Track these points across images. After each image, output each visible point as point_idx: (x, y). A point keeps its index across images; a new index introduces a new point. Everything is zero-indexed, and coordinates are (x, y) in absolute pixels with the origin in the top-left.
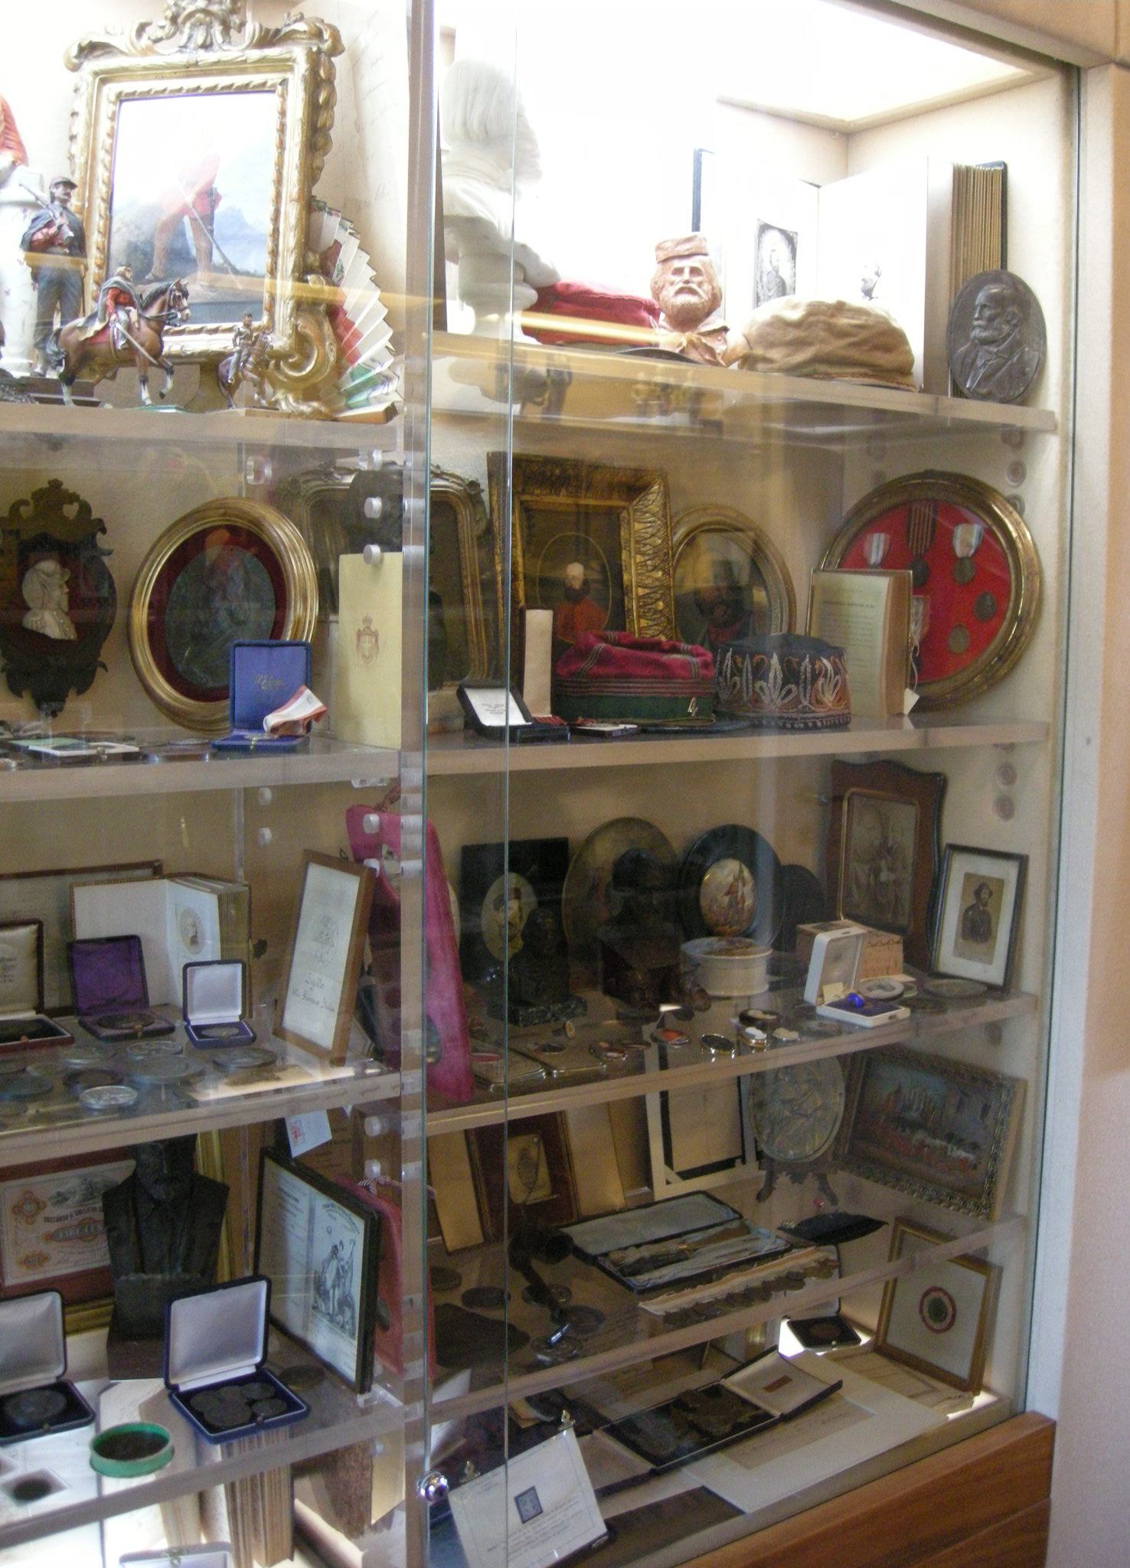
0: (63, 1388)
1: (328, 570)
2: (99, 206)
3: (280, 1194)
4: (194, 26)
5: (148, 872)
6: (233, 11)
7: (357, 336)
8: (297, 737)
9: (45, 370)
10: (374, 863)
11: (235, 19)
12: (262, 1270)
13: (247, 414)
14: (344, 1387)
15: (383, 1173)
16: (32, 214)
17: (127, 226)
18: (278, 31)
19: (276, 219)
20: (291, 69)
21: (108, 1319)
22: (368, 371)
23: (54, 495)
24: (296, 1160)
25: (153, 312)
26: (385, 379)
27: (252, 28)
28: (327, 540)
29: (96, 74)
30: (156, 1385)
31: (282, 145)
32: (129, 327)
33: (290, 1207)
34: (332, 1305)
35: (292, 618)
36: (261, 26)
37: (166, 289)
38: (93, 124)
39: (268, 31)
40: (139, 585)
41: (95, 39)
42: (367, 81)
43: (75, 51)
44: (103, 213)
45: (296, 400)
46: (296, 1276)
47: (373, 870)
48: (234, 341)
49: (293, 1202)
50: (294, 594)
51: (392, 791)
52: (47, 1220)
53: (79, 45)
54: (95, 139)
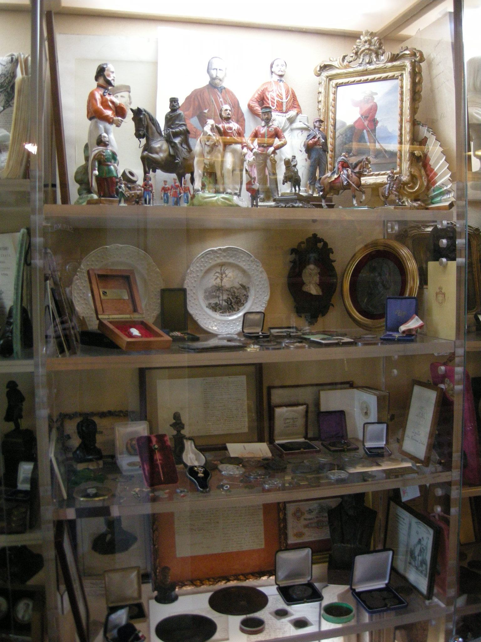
0: (310, 585)
1: (422, 267)
2: (331, 128)
3: (397, 516)
4: (364, 55)
5: (348, 385)
6: (380, 48)
7: (436, 174)
8: (413, 335)
9: (313, 193)
10: (442, 386)
11: (381, 51)
12: (387, 546)
13: (395, 208)
14: (421, 596)
15: (442, 511)
16: (306, 134)
17: (342, 135)
18: (398, 55)
19: (401, 129)
20: (404, 69)
21: (327, 559)
22: (441, 189)
23: (315, 239)
24: (403, 503)
25: (357, 170)
26: (448, 192)
27: (388, 54)
28: (422, 255)
29: (327, 77)
30: (347, 587)
31: (402, 100)
32: (348, 176)
33: (401, 522)
34: (418, 563)
35: (409, 287)
36: (391, 54)
37: (362, 161)
38: (327, 96)
39: (394, 55)
40: (346, 273)
41: (326, 63)
42: (435, 72)
43: (318, 69)
44: (332, 131)
45: (411, 201)
46: (402, 549)
47: (443, 389)
48: (387, 179)
49: (402, 520)
50: (409, 278)
51: (450, 357)
52: (305, 519)
53: (320, 66)
54: (328, 102)
